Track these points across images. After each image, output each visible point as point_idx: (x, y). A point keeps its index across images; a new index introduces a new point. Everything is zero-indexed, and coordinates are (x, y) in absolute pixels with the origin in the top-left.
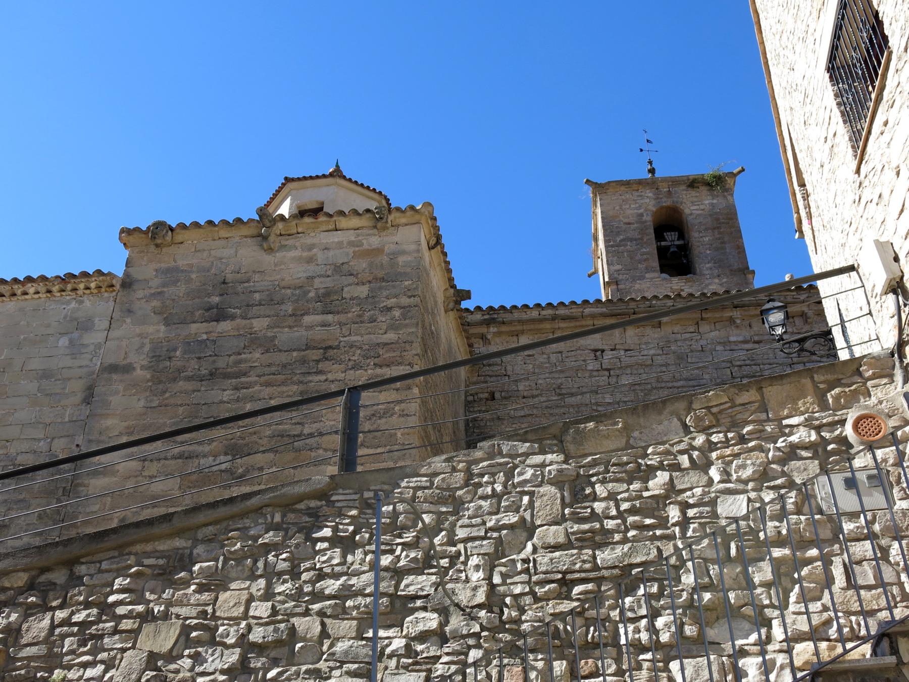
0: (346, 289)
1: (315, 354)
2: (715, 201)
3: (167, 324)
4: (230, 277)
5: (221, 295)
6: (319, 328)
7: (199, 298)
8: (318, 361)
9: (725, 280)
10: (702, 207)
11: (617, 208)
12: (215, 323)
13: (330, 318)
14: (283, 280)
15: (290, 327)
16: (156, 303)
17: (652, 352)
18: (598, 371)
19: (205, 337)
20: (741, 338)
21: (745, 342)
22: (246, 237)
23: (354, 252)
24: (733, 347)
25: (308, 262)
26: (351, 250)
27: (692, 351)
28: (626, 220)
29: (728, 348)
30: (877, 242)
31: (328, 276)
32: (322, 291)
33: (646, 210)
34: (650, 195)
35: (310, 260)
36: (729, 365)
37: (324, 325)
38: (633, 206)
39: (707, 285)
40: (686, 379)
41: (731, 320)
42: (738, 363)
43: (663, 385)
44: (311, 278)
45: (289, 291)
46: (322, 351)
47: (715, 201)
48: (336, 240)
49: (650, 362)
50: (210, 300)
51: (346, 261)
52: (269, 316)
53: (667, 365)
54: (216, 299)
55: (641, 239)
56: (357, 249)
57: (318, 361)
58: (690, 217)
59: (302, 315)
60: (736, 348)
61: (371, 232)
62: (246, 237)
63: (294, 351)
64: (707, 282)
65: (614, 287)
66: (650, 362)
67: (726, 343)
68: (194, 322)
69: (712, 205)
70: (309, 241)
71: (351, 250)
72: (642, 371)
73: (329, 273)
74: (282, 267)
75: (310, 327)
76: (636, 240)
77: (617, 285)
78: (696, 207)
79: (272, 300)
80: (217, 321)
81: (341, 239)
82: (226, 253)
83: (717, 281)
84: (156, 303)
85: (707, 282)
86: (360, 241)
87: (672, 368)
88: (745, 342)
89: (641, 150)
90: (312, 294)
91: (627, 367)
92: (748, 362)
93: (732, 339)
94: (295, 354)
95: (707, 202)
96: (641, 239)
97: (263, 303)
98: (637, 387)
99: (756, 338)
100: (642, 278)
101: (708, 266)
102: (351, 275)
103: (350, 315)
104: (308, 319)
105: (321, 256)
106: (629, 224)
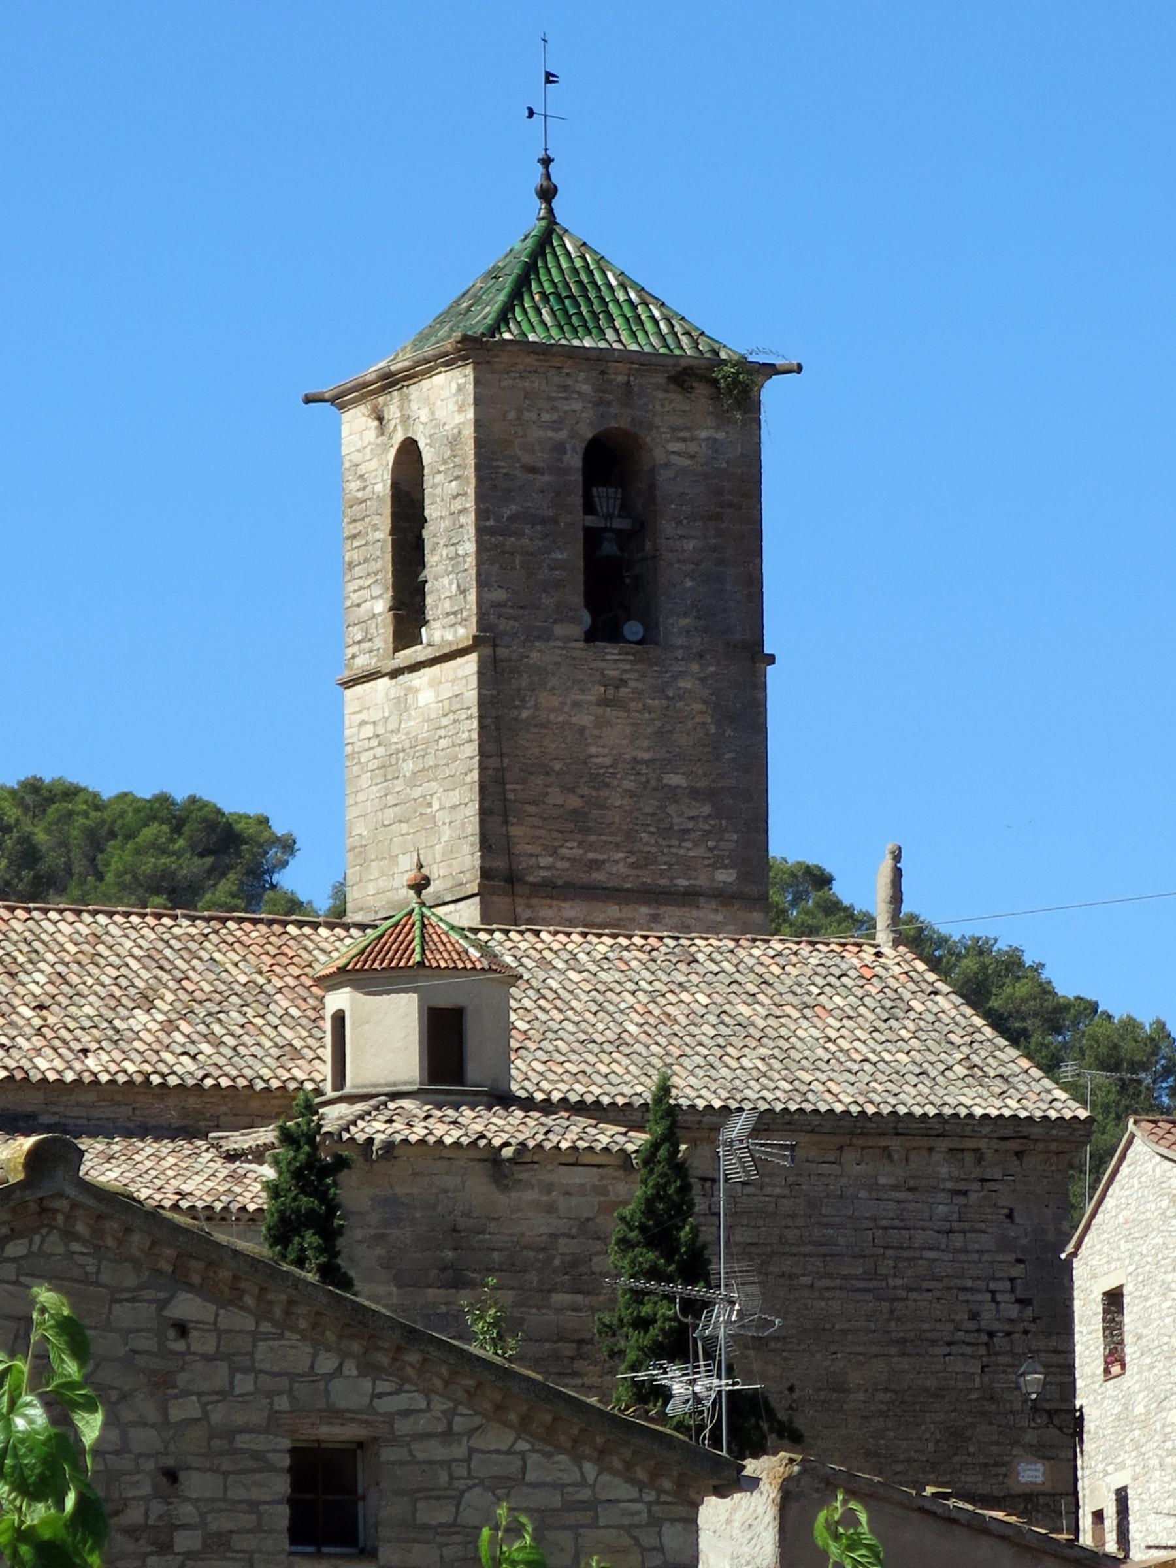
0: (595, 1259)
1: (568, 1349)
2: (721, 435)
3: (400, 1286)
4: (462, 1222)
5: (455, 1249)
6: (569, 1313)
7: (429, 1249)
8: (572, 1359)
9: (712, 669)
10: (692, 448)
11: (512, 415)
12: (454, 1291)
13: (579, 1298)
14: (523, 1235)
15: (538, 1308)
16: (379, 1251)
17: (778, 1191)
18: (705, 1214)
19: (444, 1309)
20: (892, 1181)
21: (896, 1188)
22: (472, 1160)
23: (600, 1204)
24: (881, 1195)
25: (549, 1212)
26: (596, 1200)
27: (828, 1196)
28: (527, 459)
29: (874, 1195)
30: (1121, 1287)
31: (573, 1237)
32: (568, 1258)
33: (573, 434)
34: (586, 388)
35: (551, 1208)
36: (871, 1225)
37: (576, 1309)
38: (546, 417)
39: (675, 678)
40: (818, 1244)
41: (887, 1152)
42: (884, 1223)
43: (787, 1249)
44: (554, 1236)
45: (531, 1254)
46: (574, 1345)
47: (721, 435)
48: (578, 1181)
49: (772, 1208)
50: (442, 1255)
51: (591, 1215)
52: (512, 1288)
53: (793, 1216)
54: (450, 1255)
55: (555, 520)
56: (603, 1199)
57: (572, 1359)
58: (663, 476)
59: (549, 1291)
60: (885, 1196)
61: (616, 1174)
62: (472, 1160)
63: (546, 1340)
64: (677, 668)
65: (488, 651)
66: (772, 1208)
67: (873, 1186)
68: (429, 1286)
69: (713, 442)
70: (546, 1177)
71: (596, 1200)
72: (761, 1222)
73: (574, 1231)
74: (519, 1215)
75: (560, 1310)
76: (543, 521)
77: (495, 646)
78: (676, 443)
79: (513, 1265)
80: (456, 1287)
81: (583, 1181)
82: (451, 1182)
83: (695, 667)
84: (379, 1251)
85: (677, 668)
86: (605, 1187)
87: (800, 1222)
88: (896, 1188)
89: (531, 113)
90: (557, 1262)
91: (743, 1213)
92: (897, 1223)
93: (882, 1180)
94: (547, 1346)
95: (703, 434)
96: (555, 520)
97: (504, 1267)
98: (753, 1249)
99: (912, 1183)
100: (546, 635)
101: (684, 622)
102: (599, 1239)
103: (601, 1298)
104: (558, 1298)
105: (562, 1204)
106: (533, 470)
